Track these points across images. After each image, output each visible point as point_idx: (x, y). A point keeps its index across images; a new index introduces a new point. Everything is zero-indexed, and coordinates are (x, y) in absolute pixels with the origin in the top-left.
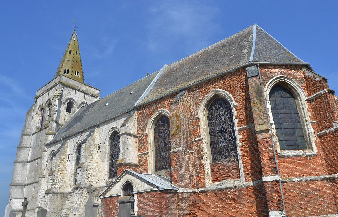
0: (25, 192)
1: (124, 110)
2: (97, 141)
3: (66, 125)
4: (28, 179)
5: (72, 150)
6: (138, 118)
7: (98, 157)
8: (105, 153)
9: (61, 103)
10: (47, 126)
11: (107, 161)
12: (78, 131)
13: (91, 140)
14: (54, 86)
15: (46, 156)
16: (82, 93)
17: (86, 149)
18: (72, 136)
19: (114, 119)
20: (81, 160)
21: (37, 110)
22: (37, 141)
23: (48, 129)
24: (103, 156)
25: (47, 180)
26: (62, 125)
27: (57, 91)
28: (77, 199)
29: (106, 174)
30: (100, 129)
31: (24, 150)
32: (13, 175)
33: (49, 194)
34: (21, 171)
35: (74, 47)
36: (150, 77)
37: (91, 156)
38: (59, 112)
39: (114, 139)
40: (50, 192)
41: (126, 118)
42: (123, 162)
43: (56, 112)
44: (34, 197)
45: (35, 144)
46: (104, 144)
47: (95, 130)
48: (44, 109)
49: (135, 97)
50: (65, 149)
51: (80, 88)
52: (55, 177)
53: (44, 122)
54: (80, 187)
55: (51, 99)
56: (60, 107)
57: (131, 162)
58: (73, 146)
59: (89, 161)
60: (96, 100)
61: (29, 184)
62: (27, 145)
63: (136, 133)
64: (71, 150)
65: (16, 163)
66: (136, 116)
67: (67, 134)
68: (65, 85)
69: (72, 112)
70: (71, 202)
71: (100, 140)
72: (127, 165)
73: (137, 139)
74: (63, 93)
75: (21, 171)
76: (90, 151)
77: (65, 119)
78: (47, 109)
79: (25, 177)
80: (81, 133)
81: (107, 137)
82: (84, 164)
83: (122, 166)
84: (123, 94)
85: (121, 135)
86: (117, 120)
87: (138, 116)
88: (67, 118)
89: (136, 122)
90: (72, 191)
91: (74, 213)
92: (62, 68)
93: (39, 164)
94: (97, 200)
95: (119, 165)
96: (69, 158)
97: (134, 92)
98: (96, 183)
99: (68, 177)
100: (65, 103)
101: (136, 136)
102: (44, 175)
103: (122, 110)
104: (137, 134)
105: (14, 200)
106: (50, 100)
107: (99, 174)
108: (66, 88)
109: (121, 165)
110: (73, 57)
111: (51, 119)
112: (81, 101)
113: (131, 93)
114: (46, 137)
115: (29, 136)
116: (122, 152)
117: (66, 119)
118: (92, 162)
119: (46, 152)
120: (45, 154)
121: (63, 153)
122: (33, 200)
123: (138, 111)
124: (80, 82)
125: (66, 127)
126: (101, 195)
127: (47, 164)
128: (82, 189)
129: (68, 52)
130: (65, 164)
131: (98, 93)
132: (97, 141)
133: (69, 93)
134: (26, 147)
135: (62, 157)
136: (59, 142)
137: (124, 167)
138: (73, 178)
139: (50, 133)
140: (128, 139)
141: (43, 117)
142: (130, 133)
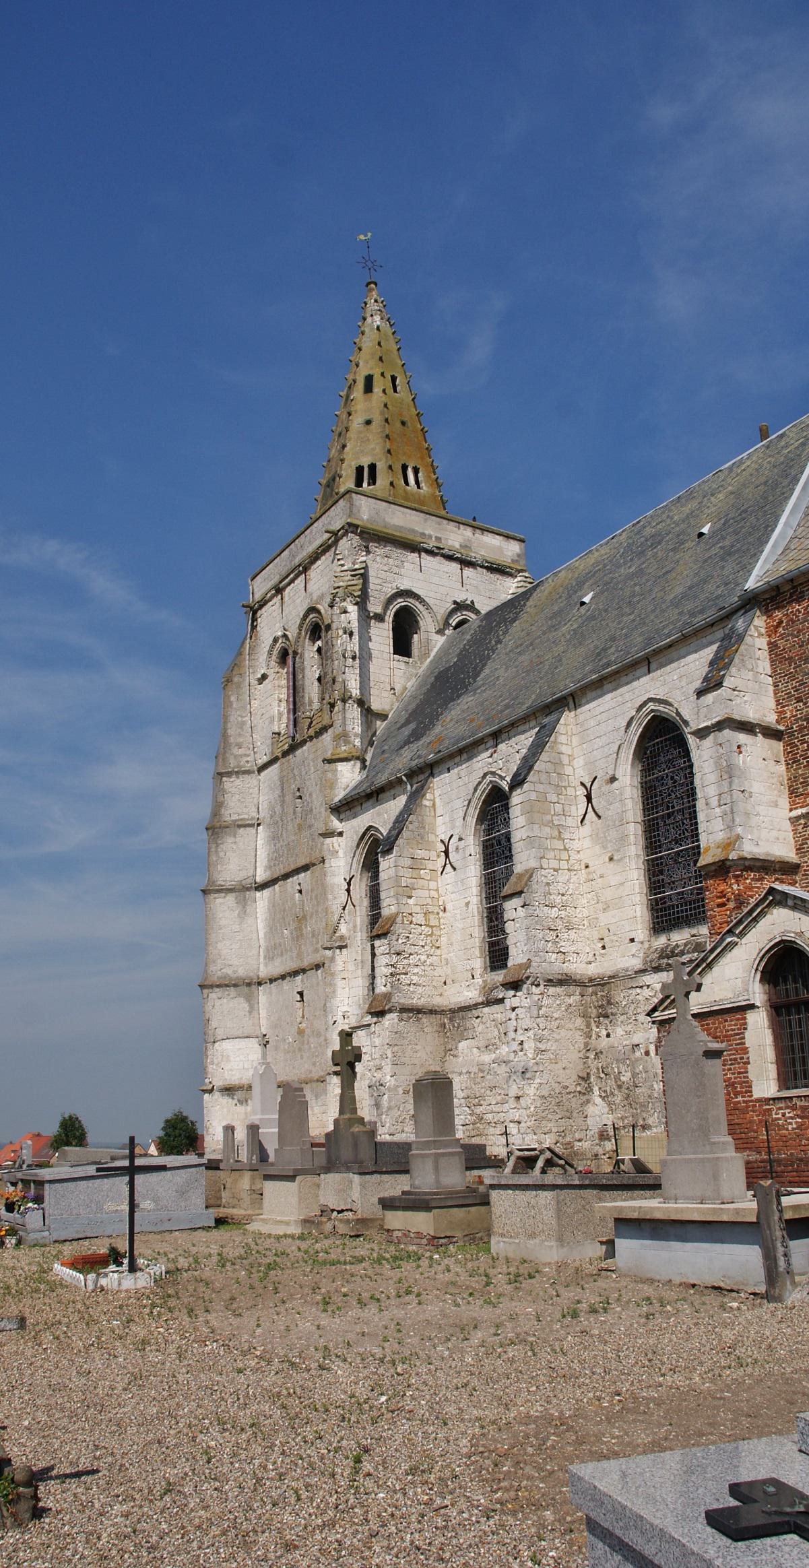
0: (263, 1013)
1: (692, 614)
2: (578, 771)
3: (405, 715)
4: (270, 958)
5: (459, 822)
6: (772, 646)
7: (587, 843)
8: (623, 823)
9: (366, 618)
10: (320, 726)
11: (638, 856)
12: (473, 734)
13: (549, 767)
14: (325, 549)
15: (341, 854)
16: (447, 563)
17: (530, 810)
18: (451, 756)
19: (648, 662)
20: (516, 858)
21: (262, 660)
22: (283, 795)
23: (327, 737)
24: (613, 834)
25: (359, 958)
26: (383, 717)
27: (342, 565)
28: (520, 1031)
29: (639, 914)
30: (581, 718)
31: (235, 837)
32: (206, 943)
33: (388, 1016)
34: (236, 927)
35: (381, 359)
36: (783, 443)
37: (560, 838)
38: (364, 657)
39: (655, 755)
40: (391, 1005)
41: (714, 647)
42: (733, 856)
43: (354, 658)
44: (308, 1031)
45: (278, 809)
46: (613, 779)
47: (562, 721)
48: (295, 653)
49: (732, 546)
50: (428, 820)
51: (438, 539)
52: (400, 941)
53: (302, 709)
54: (528, 978)
55: (319, 606)
56: (365, 639)
57: (768, 855)
58: (460, 804)
59: (554, 864)
60: (510, 587)
61: (276, 980)
62: (246, 817)
63: (771, 719)
64: (452, 821)
65: (213, 896)
66: (761, 635)
67: (423, 752)
68: (372, 537)
69: (415, 651)
70: (482, 1043)
71: (589, 764)
72: (749, 869)
73: (779, 746)
74: (372, 573)
75: (236, 927)
76: (549, 817)
77: (393, 689)
78: (309, 652)
79: (255, 952)
80: (491, 743)
81: (624, 747)
82: (531, 876)
83: (730, 875)
84: (659, 543)
85: (702, 734)
86: (661, 666)
87: (769, 636)
88: (403, 681)
89: (765, 666)
90: (480, 1000)
91: (514, 1091)
92: (342, 461)
93: (307, 892)
94: (604, 1033)
95: (713, 868)
96: (447, 855)
97: (718, 525)
98: (591, 958)
99: (457, 937)
100: (385, 614)
101: (773, 730)
102: (342, 938)
103: (681, 613)
104: (778, 722)
105: (227, 1045)
106: (319, 612)
107: (605, 919)
108: (379, 551)
109: (722, 869)
110: (386, 405)
111: (336, 695)
112: (450, 600)
113: (701, 535)
114: (330, 775)
115: (246, 776)
116: (718, 810)
117: (398, 687)
118: (564, 865)
119: (340, 839)
120: (336, 845)
121: (422, 838)
122: (303, 1043)
123: (767, 612)
124: (431, 511)
125: (408, 722)
126: (654, 1010)
127: (348, 890)
128: (538, 985)
129: (360, 385)
130: (433, 885)
131: (519, 556)
132: (578, 771)
133: (397, 570)
134: (240, 826)
135: (420, 854)
136: (392, 792)
137: (736, 877)
138: (477, 940)
139: (342, 756)
140: (739, 747)
141: (295, 690)
142: (747, 719)
